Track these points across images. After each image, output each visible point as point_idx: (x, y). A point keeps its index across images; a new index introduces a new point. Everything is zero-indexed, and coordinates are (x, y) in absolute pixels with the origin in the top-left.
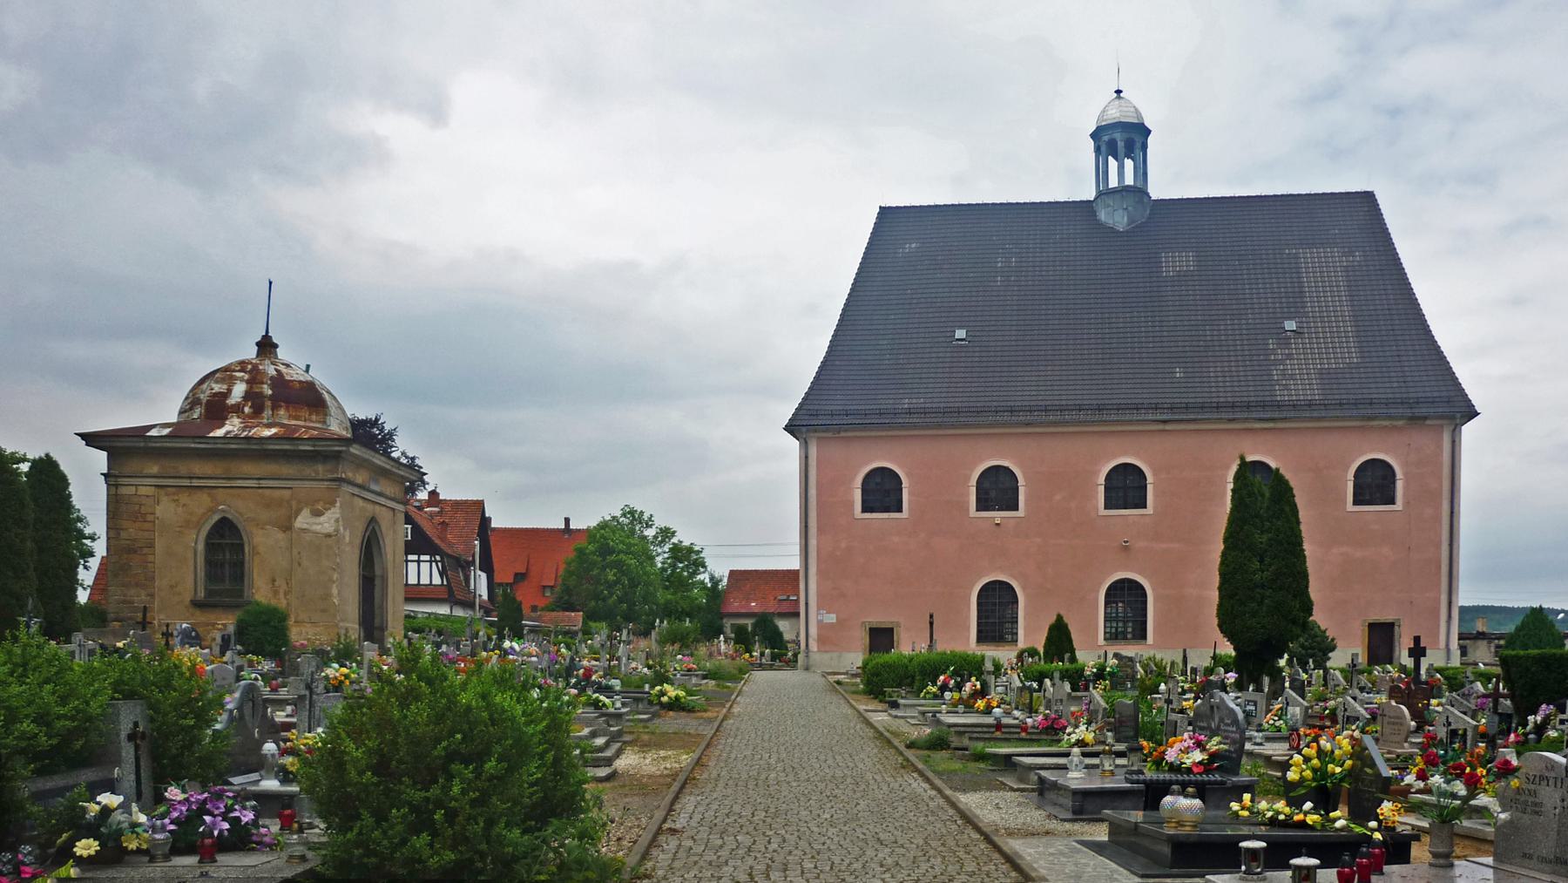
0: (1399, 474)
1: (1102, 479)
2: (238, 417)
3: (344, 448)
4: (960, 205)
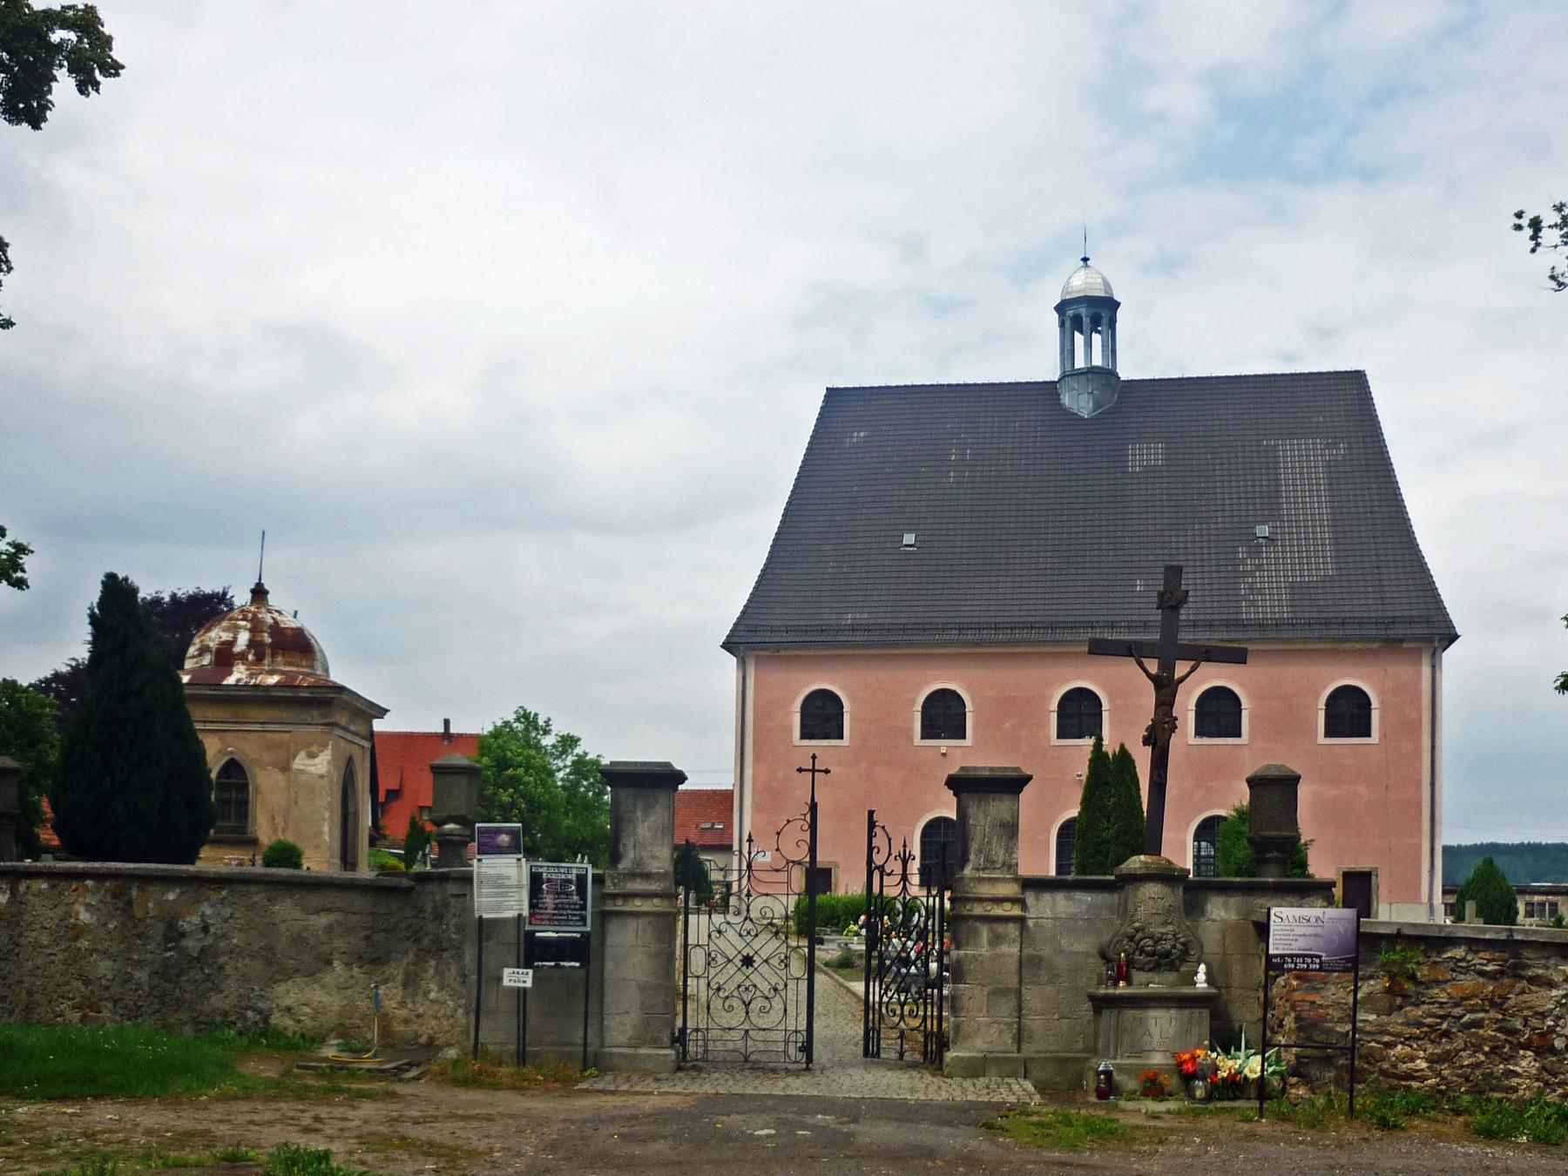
0: (1375, 703)
1: (1054, 706)
2: (243, 664)
4: (912, 386)
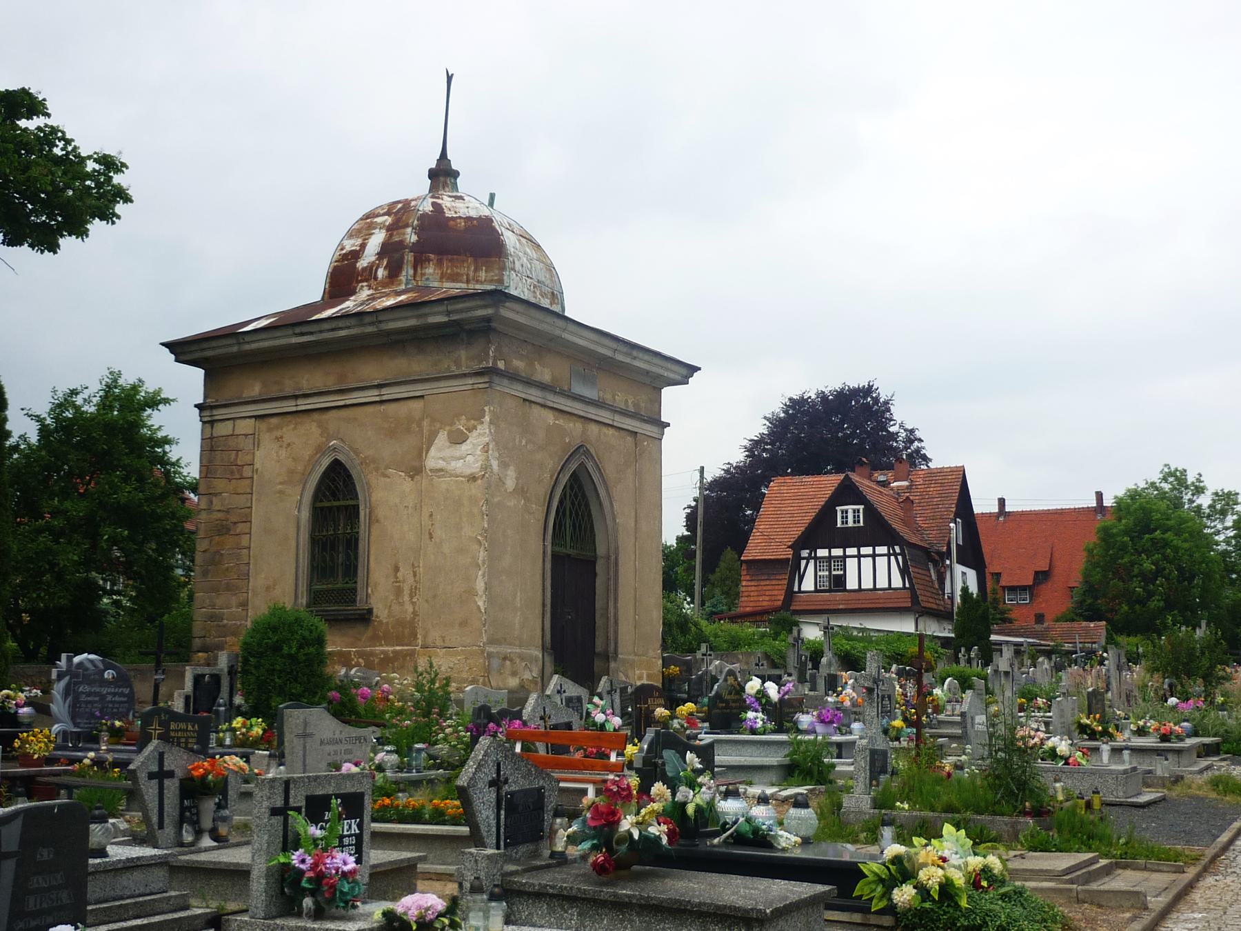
3: (490, 311)
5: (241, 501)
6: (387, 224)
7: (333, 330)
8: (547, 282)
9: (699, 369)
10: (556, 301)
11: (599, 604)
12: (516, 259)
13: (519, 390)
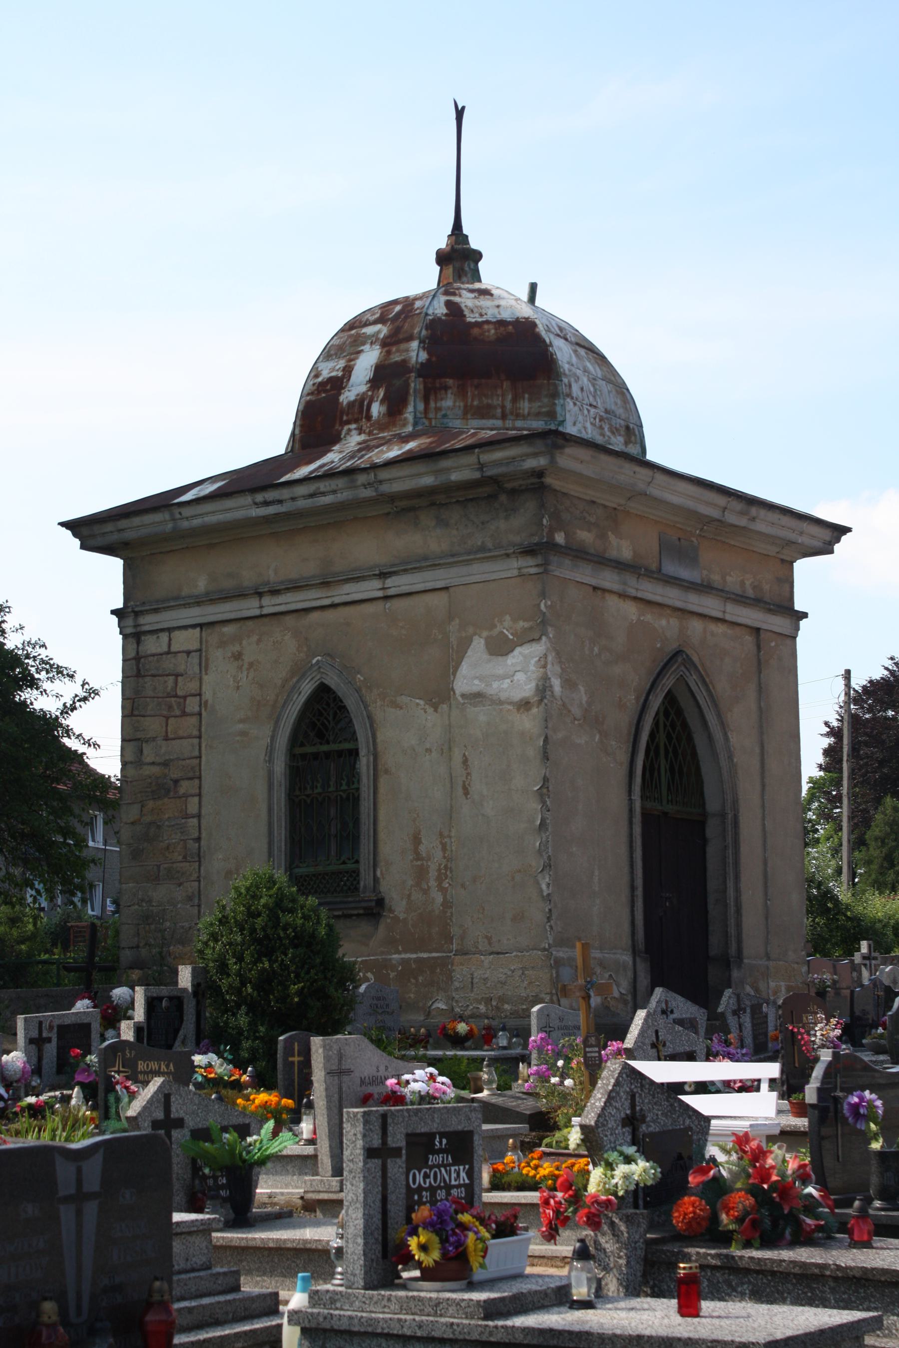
3: (542, 462)
5: (185, 747)
6: (381, 336)
7: (312, 496)
8: (620, 411)
9: (849, 530)
10: (633, 438)
11: (712, 885)
12: (572, 380)
13: (585, 574)
